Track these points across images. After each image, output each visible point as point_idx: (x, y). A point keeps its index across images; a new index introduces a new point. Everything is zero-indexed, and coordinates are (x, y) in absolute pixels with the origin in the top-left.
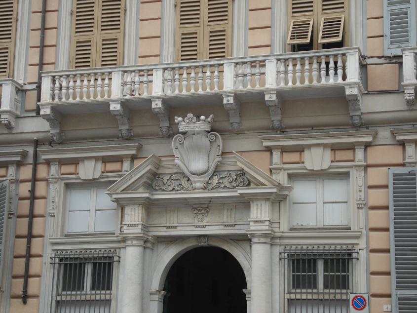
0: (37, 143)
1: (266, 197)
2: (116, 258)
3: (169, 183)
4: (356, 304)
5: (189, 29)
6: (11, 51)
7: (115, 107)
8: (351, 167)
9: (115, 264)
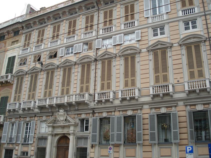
4: (111, 148)
5: (191, 70)
6: (89, 86)
8: (89, 117)
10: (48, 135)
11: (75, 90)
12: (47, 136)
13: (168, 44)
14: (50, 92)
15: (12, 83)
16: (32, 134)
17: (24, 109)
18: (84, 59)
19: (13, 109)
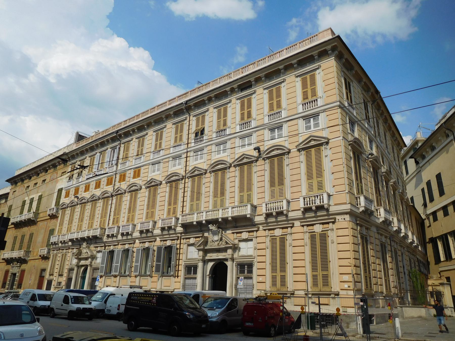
0: (181, 233)
1: (230, 248)
7: (195, 223)
10: (199, 261)
11: (207, 205)
12: (74, 267)
13: (323, 140)
14: (198, 205)
15: (58, 216)
16: (116, 264)
18: (172, 176)
19: (126, 232)
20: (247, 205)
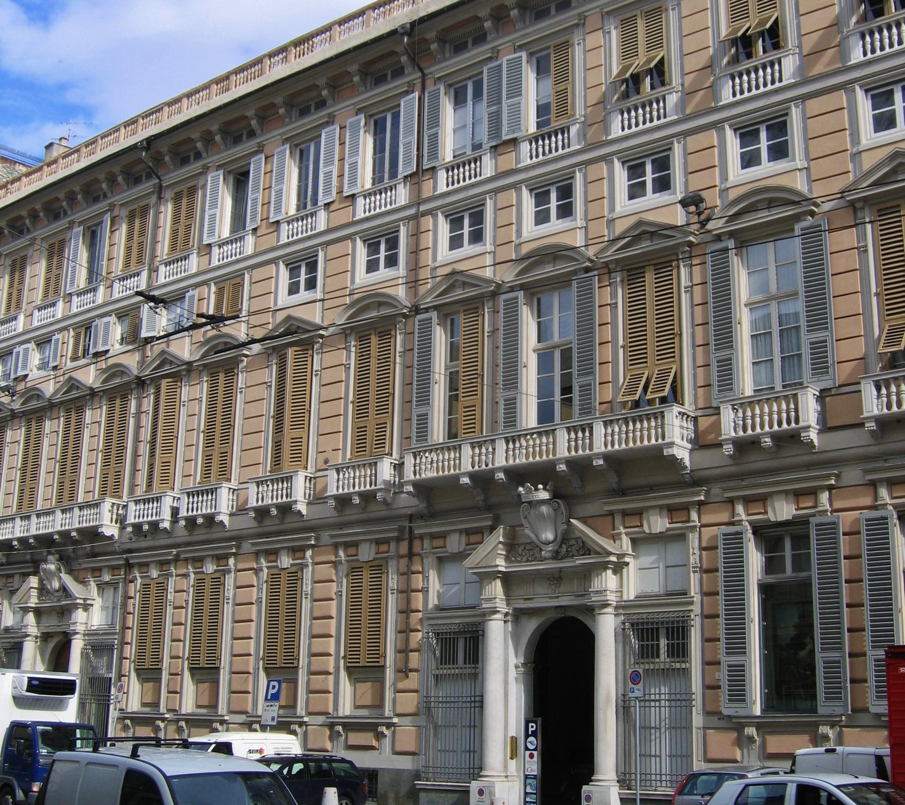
0: (411, 518)
2: (481, 633)
3: (524, 554)
8: (687, 528)
9: (481, 637)
13: (679, 235)
17: (191, 522)
20: (291, 476)
